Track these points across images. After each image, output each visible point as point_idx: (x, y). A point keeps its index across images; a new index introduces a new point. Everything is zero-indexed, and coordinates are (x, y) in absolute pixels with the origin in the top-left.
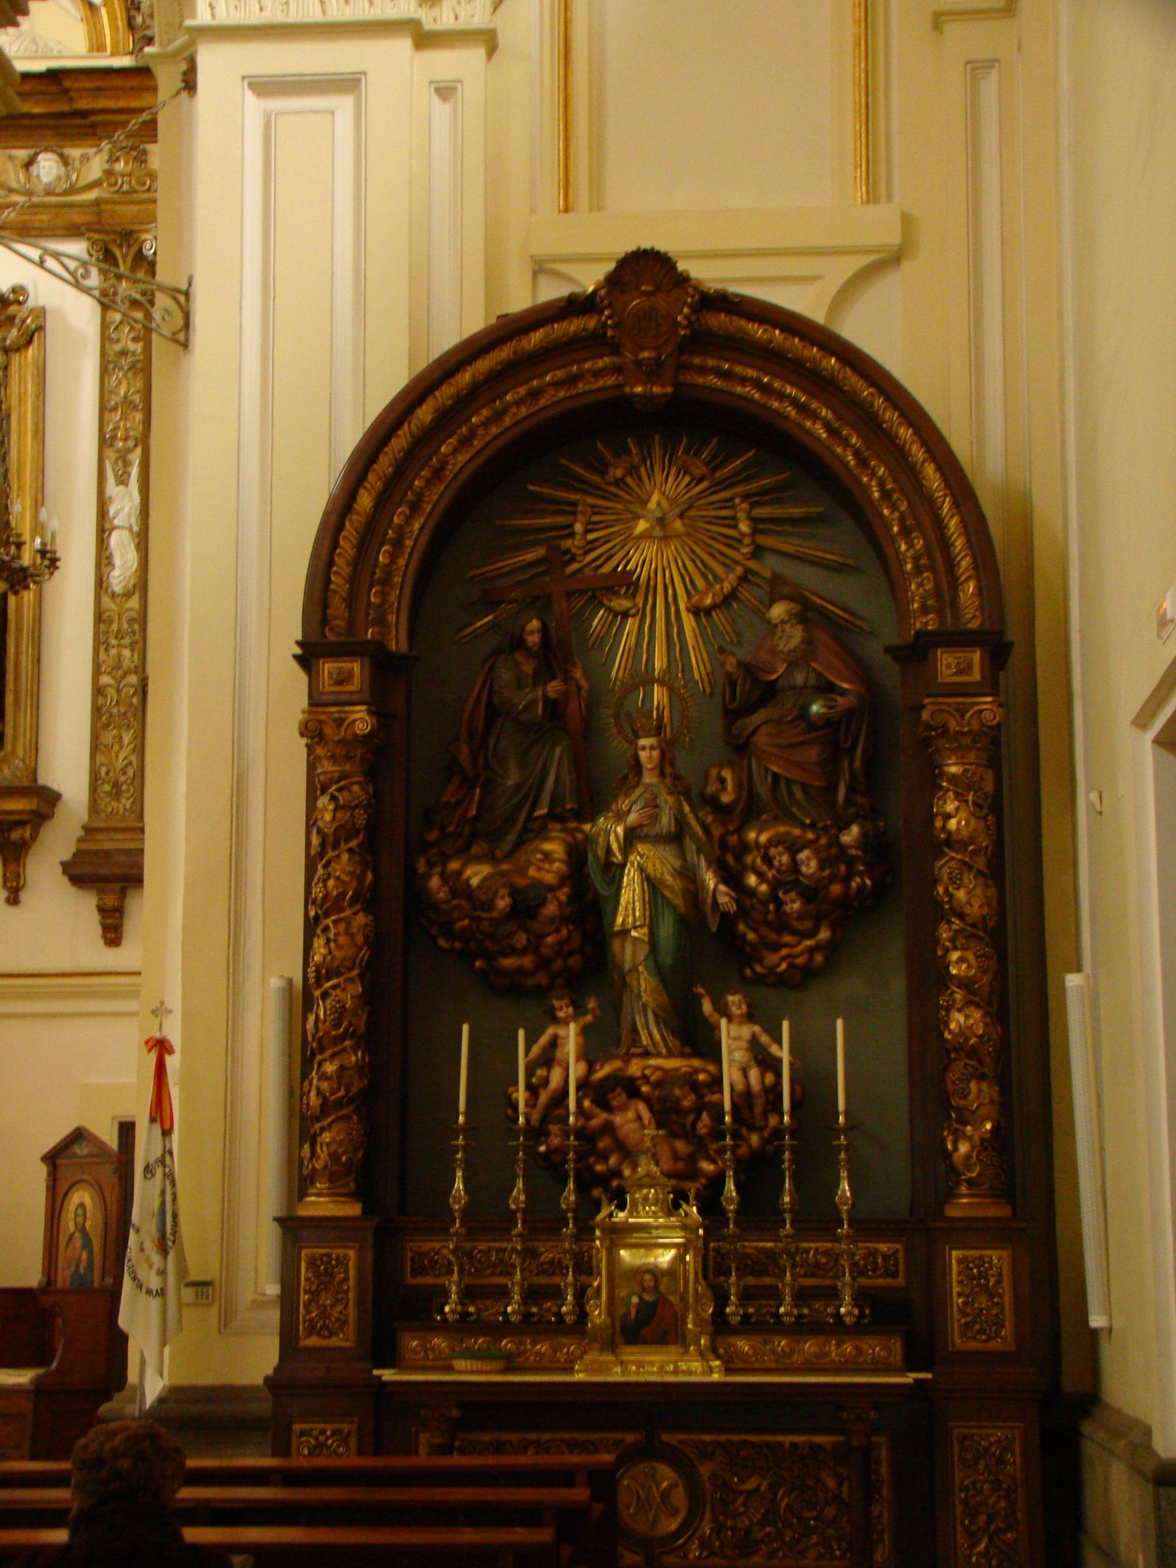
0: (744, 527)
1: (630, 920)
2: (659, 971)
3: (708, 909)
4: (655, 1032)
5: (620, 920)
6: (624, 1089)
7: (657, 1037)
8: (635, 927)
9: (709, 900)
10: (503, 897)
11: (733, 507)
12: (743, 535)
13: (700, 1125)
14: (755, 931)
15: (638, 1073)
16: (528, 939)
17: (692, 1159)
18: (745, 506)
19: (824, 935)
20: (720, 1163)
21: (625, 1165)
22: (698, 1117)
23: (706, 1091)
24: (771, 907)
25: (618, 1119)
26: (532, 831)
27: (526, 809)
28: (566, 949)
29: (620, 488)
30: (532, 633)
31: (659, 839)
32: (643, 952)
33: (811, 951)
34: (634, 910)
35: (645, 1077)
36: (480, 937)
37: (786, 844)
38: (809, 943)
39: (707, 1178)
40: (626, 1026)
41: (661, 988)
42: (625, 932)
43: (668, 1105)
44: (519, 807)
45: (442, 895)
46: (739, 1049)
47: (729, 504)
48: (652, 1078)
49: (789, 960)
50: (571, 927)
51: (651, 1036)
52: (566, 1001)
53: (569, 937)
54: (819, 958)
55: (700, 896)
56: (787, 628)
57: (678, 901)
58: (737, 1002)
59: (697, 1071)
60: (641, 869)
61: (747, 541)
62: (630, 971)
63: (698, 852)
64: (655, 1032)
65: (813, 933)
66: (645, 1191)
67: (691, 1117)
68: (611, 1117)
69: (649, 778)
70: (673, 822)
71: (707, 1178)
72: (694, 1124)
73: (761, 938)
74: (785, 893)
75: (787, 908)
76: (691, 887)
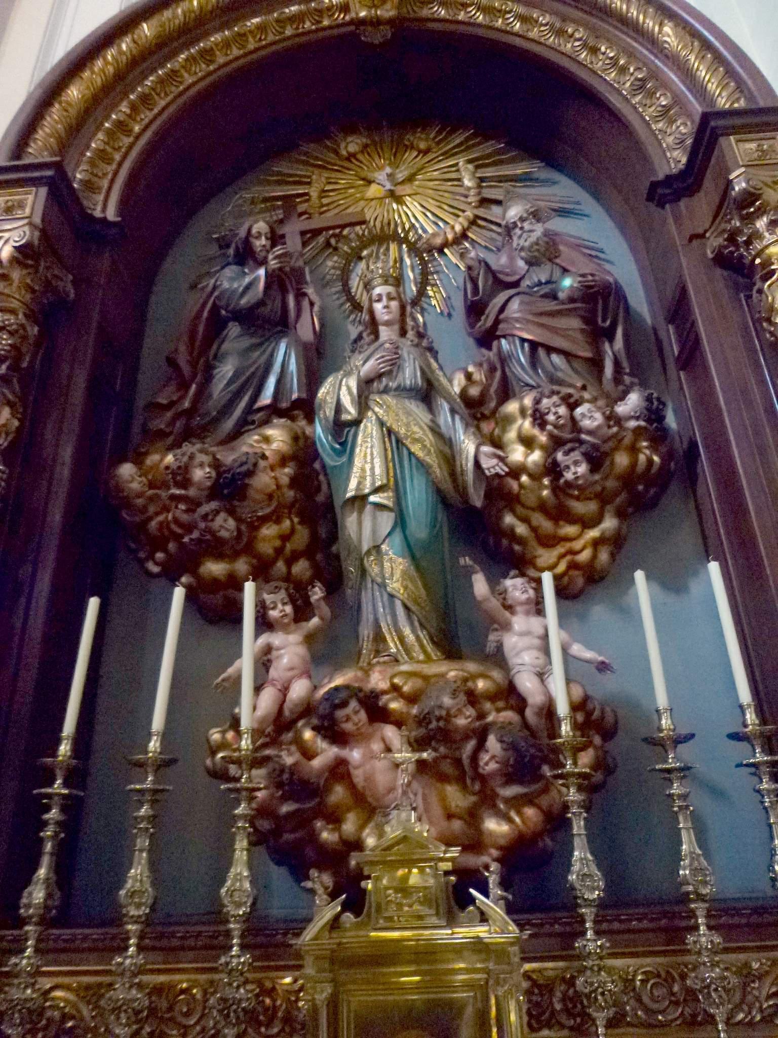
0: (467, 182)
1: (368, 482)
2: (411, 551)
3: (470, 476)
4: (407, 631)
5: (353, 484)
6: (361, 702)
7: (410, 637)
8: (376, 490)
9: (470, 464)
10: (201, 465)
11: (458, 171)
12: (469, 189)
13: (485, 757)
14: (525, 520)
15: (384, 685)
16: (239, 530)
17: (473, 817)
18: (470, 167)
19: (609, 523)
20: (517, 820)
21: (367, 831)
22: (481, 746)
23: (488, 706)
24: (546, 481)
25: (355, 755)
26: (253, 422)
27: (246, 399)
28: (289, 547)
29: (351, 161)
30: (259, 235)
31: (403, 391)
32: (386, 521)
33: (596, 544)
34: (372, 469)
35: (395, 688)
36: (179, 531)
37: (561, 395)
38: (594, 533)
39: (500, 848)
40: (366, 631)
41: (412, 571)
42: (360, 500)
43: (433, 725)
44: (237, 395)
45: (135, 486)
46: (528, 648)
47: (454, 169)
48: (406, 689)
49: (569, 558)
50: (296, 520)
51: (402, 639)
52: (282, 594)
53: (293, 531)
54: (604, 556)
55: (458, 463)
56: (526, 226)
57: (432, 460)
58: (520, 587)
59: (474, 677)
60: (382, 424)
61: (472, 192)
62: (368, 553)
63: (453, 411)
64: (407, 631)
65: (595, 521)
66: (400, 872)
67: (471, 745)
68: (345, 753)
69: (385, 333)
70: (419, 374)
71: (500, 848)
72: (474, 758)
73: (534, 529)
74: (567, 453)
75: (569, 476)
76: (447, 450)
